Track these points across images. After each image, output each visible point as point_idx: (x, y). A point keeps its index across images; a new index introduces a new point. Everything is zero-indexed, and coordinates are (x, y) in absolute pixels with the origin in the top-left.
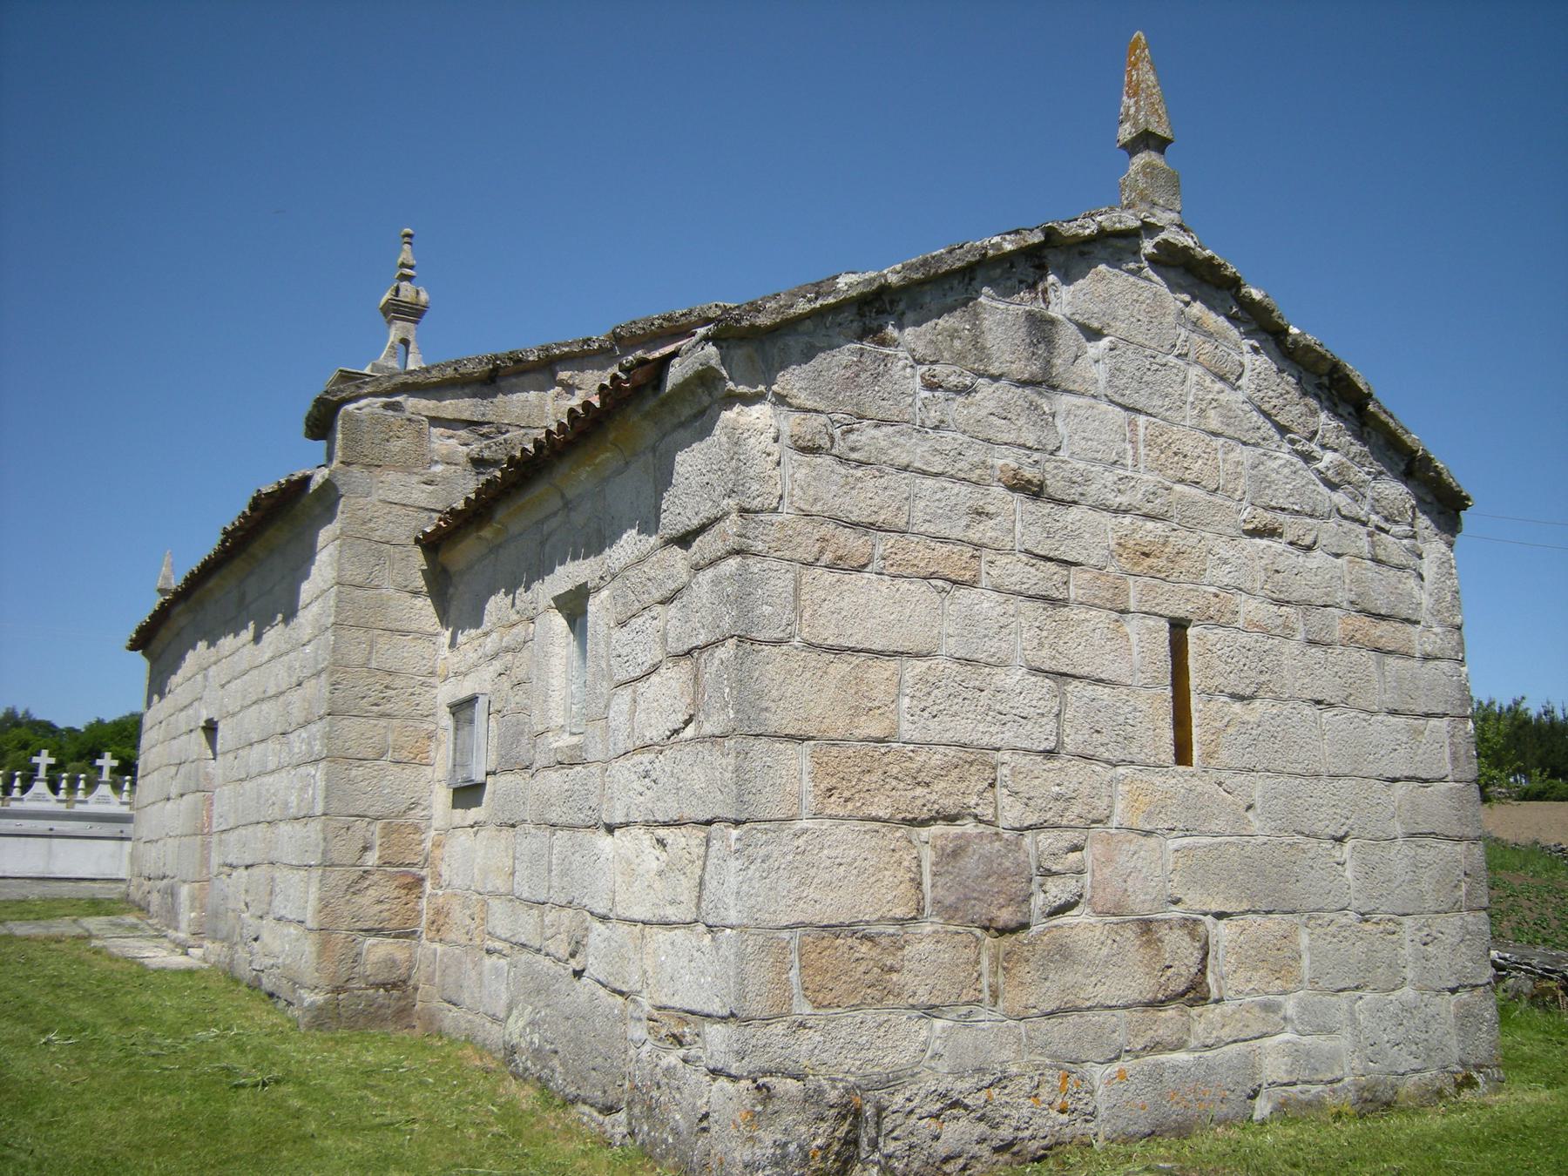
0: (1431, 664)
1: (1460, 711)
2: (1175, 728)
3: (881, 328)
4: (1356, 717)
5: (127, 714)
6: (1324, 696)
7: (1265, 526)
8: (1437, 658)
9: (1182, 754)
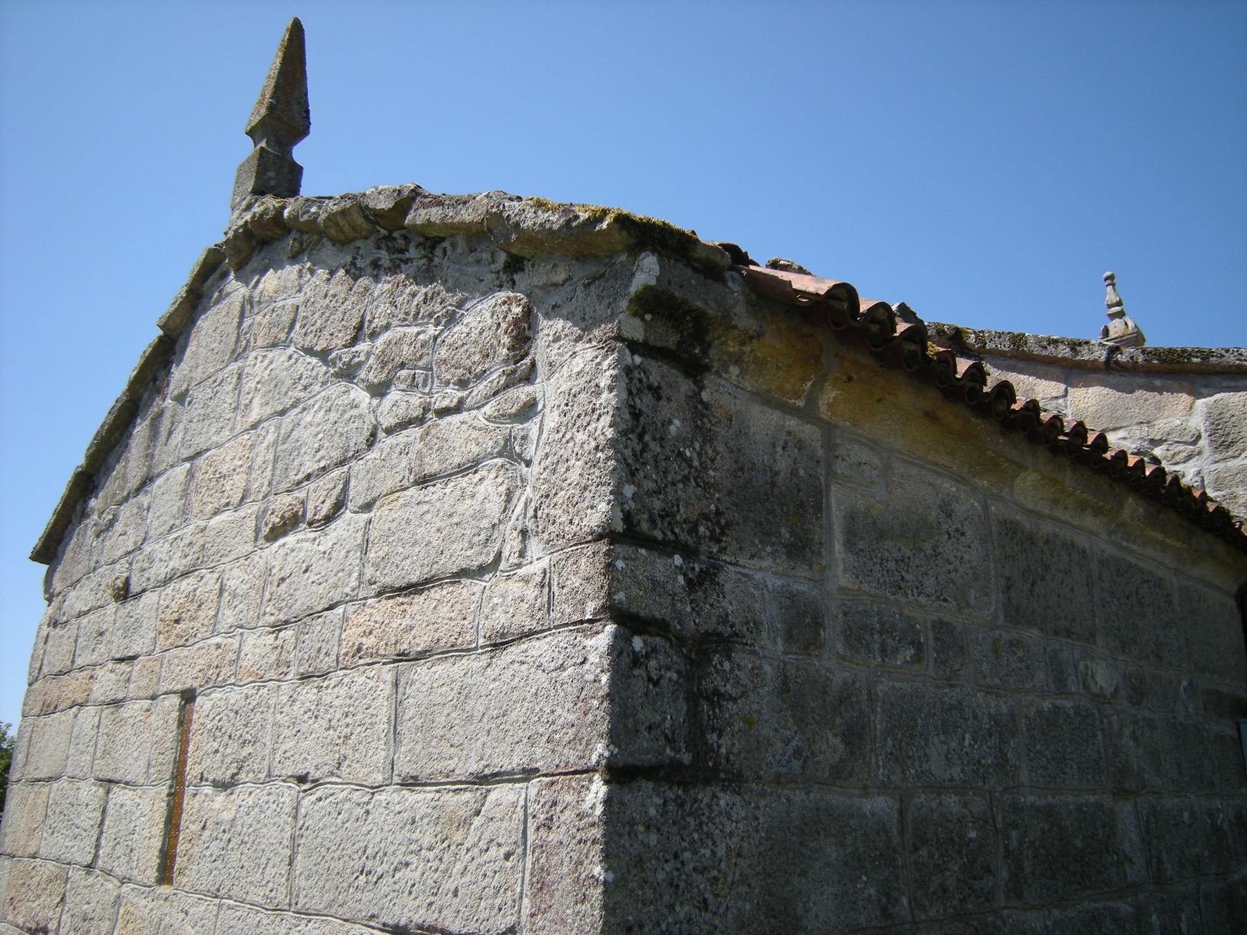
0: (514, 652)
1: (571, 756)
2: (165, 836)
3: (6, 750)
4: (347, 800)
5: (1167, 347)
6: (308, 767)
7: (282, 517)
8: (528, 635)
9: (166, 873)
